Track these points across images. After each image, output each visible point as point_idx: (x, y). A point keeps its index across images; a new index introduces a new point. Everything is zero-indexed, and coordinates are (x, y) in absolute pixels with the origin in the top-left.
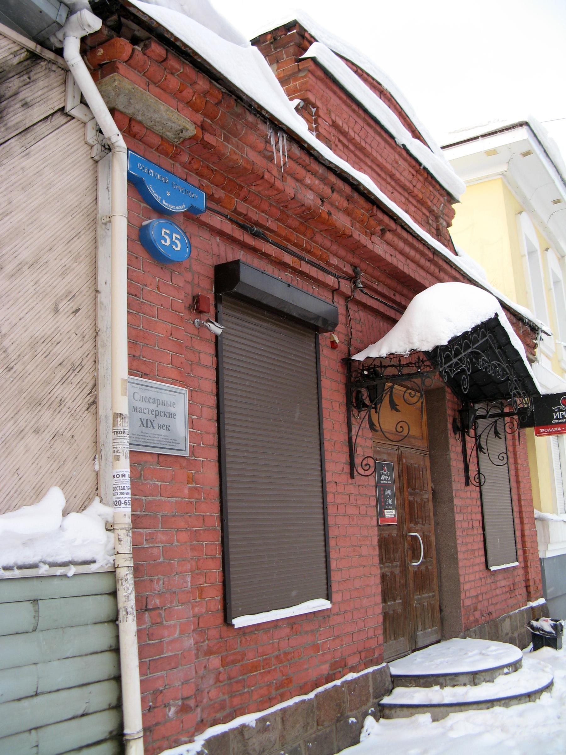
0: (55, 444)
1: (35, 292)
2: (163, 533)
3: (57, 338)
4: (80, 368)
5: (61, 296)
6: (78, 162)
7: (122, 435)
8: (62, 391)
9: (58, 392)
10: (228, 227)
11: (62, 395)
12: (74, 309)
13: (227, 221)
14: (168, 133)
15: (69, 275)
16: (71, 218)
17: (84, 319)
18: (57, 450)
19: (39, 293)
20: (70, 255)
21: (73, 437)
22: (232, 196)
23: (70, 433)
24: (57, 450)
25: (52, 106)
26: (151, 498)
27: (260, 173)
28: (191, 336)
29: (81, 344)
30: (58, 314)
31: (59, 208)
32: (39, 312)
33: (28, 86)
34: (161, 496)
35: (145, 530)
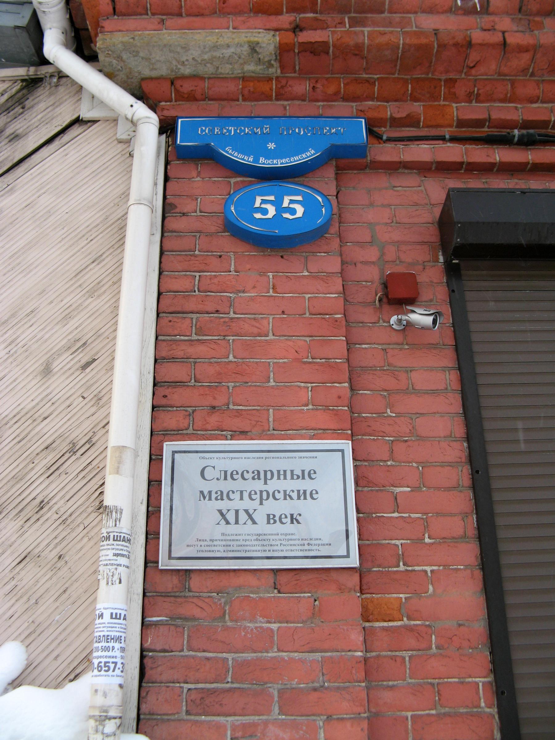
0: (23, 573)
1: (7, 356)
2: (282, 725)
3: (46, 410)
4: (87, 446)
5: (60, 349)
6: (105, 169)
7: (105, 543)
8: (47, 487)
9: (40, 489)
10: (453, 153)
11: (45, 493)
12: (83, 361)
13: (449, 144)
14: (247, 68)
15: (76, 319)
16: (86, 242)
17: (104, 371)
18: (24, 582)
19: (15, 356)
20: (80, 289)
21: (60, 557)
22: (442, 103)
23: (55, 553)
24: (24, 582)
25: (59, 123)
26: (249, 656)
27: (459, 38)
28: (384, 347)
29: (93, 409)
30: (49, 376)
31: (64, 236)
32: (15, 381)
33: (23, 115)
34: (279, 650)
35: (230, 719)
